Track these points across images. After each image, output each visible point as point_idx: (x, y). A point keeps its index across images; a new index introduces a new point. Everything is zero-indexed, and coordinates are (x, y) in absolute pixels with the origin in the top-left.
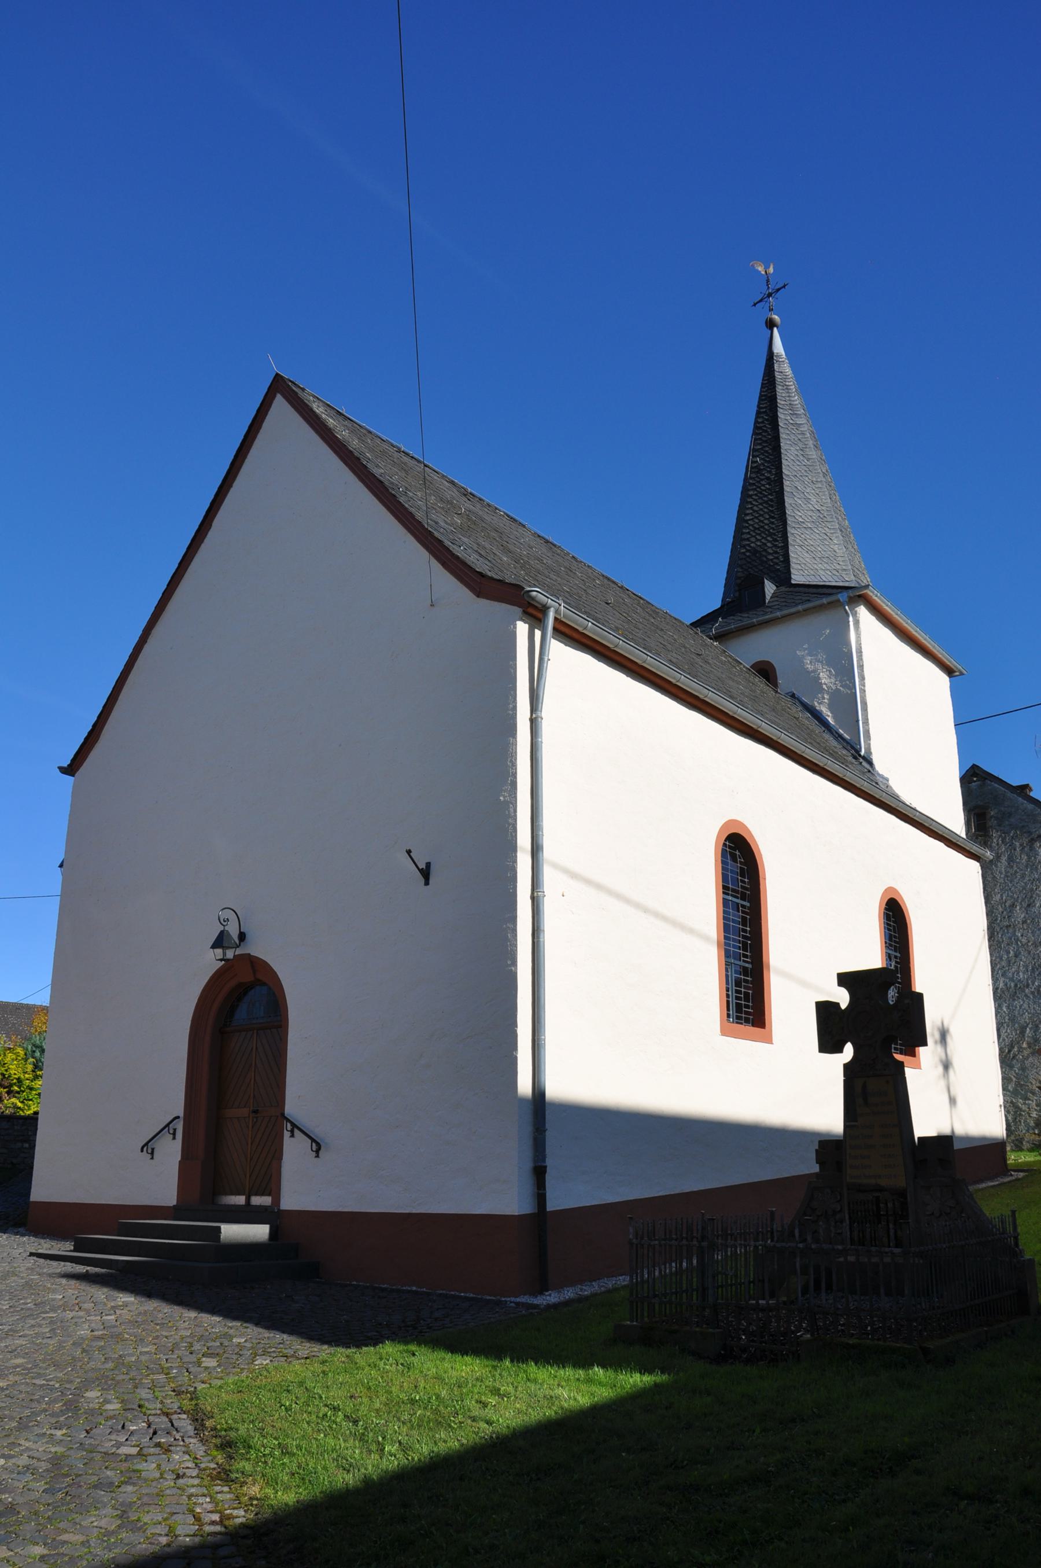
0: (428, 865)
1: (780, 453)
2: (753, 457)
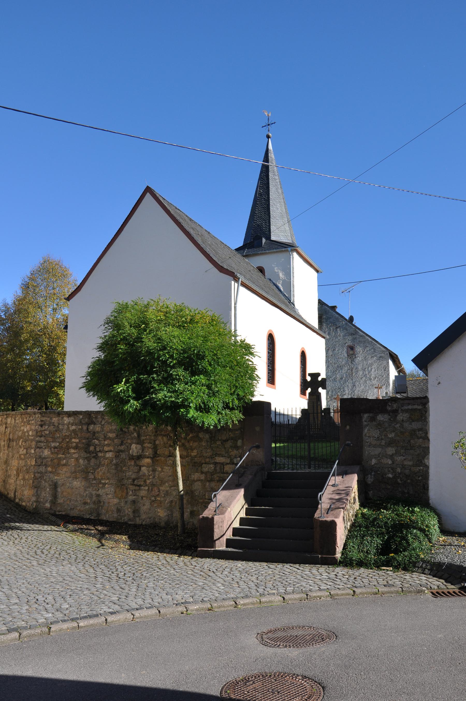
2: (259, 189)
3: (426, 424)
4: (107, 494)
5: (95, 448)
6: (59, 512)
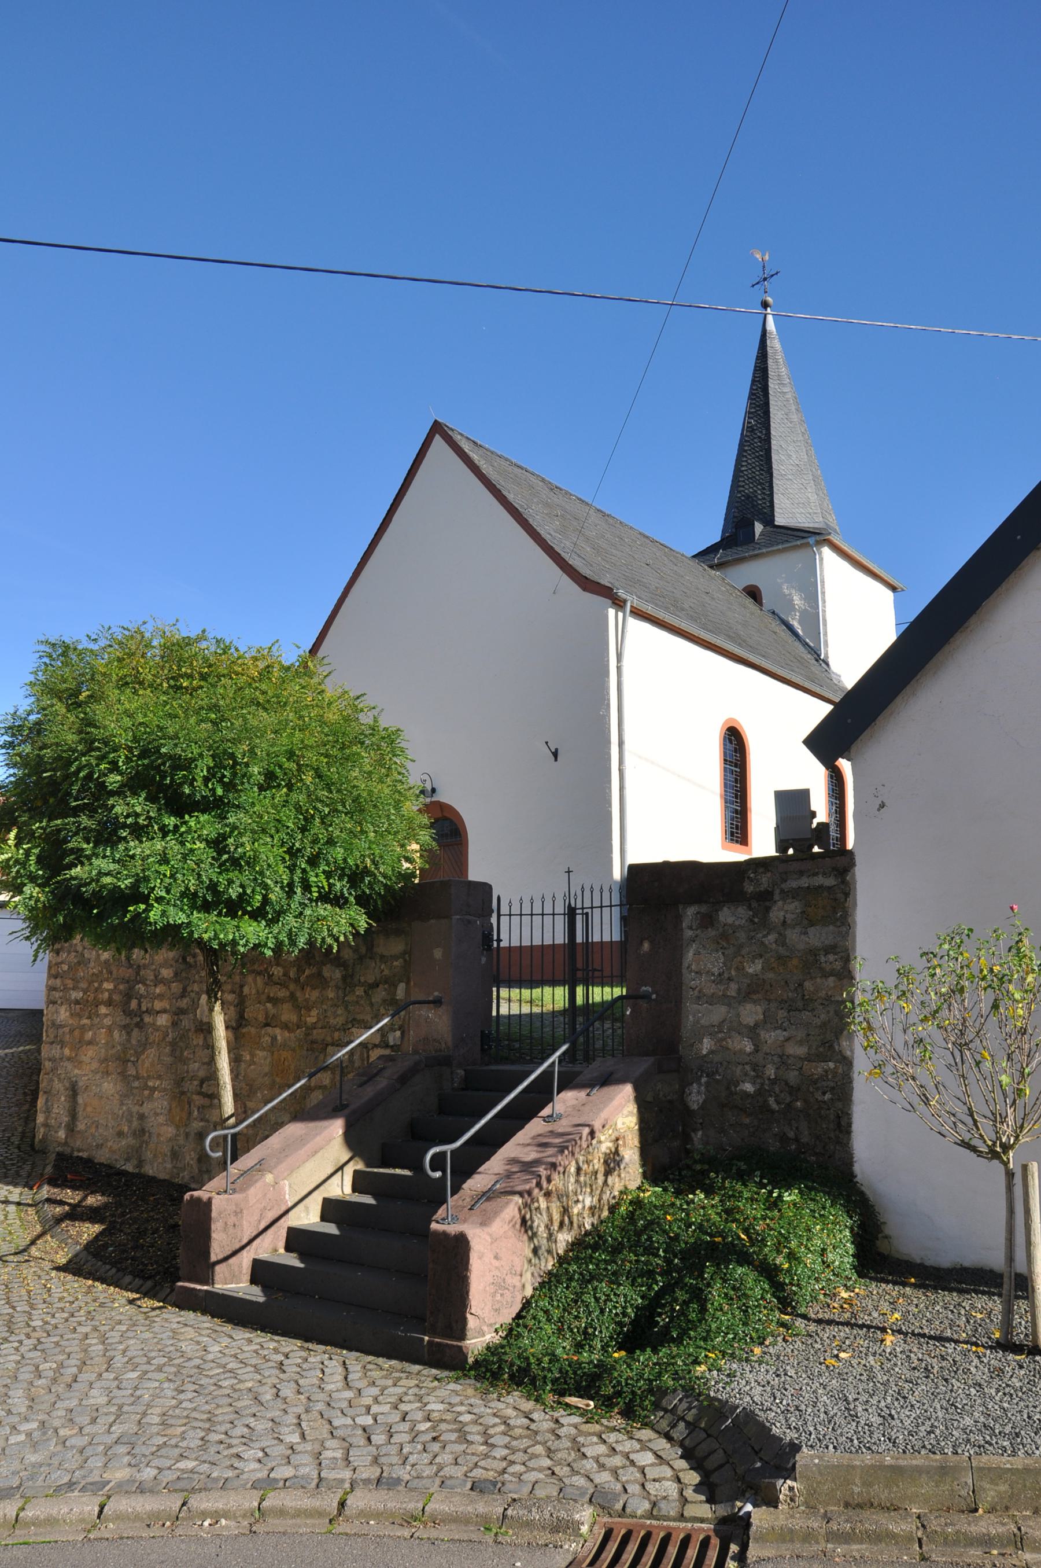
0: (557, 750)
1: (769, 417)
3: (847, 933)
4: (156, 1114)
5: (139, 1005)
6: (79, 1151)
